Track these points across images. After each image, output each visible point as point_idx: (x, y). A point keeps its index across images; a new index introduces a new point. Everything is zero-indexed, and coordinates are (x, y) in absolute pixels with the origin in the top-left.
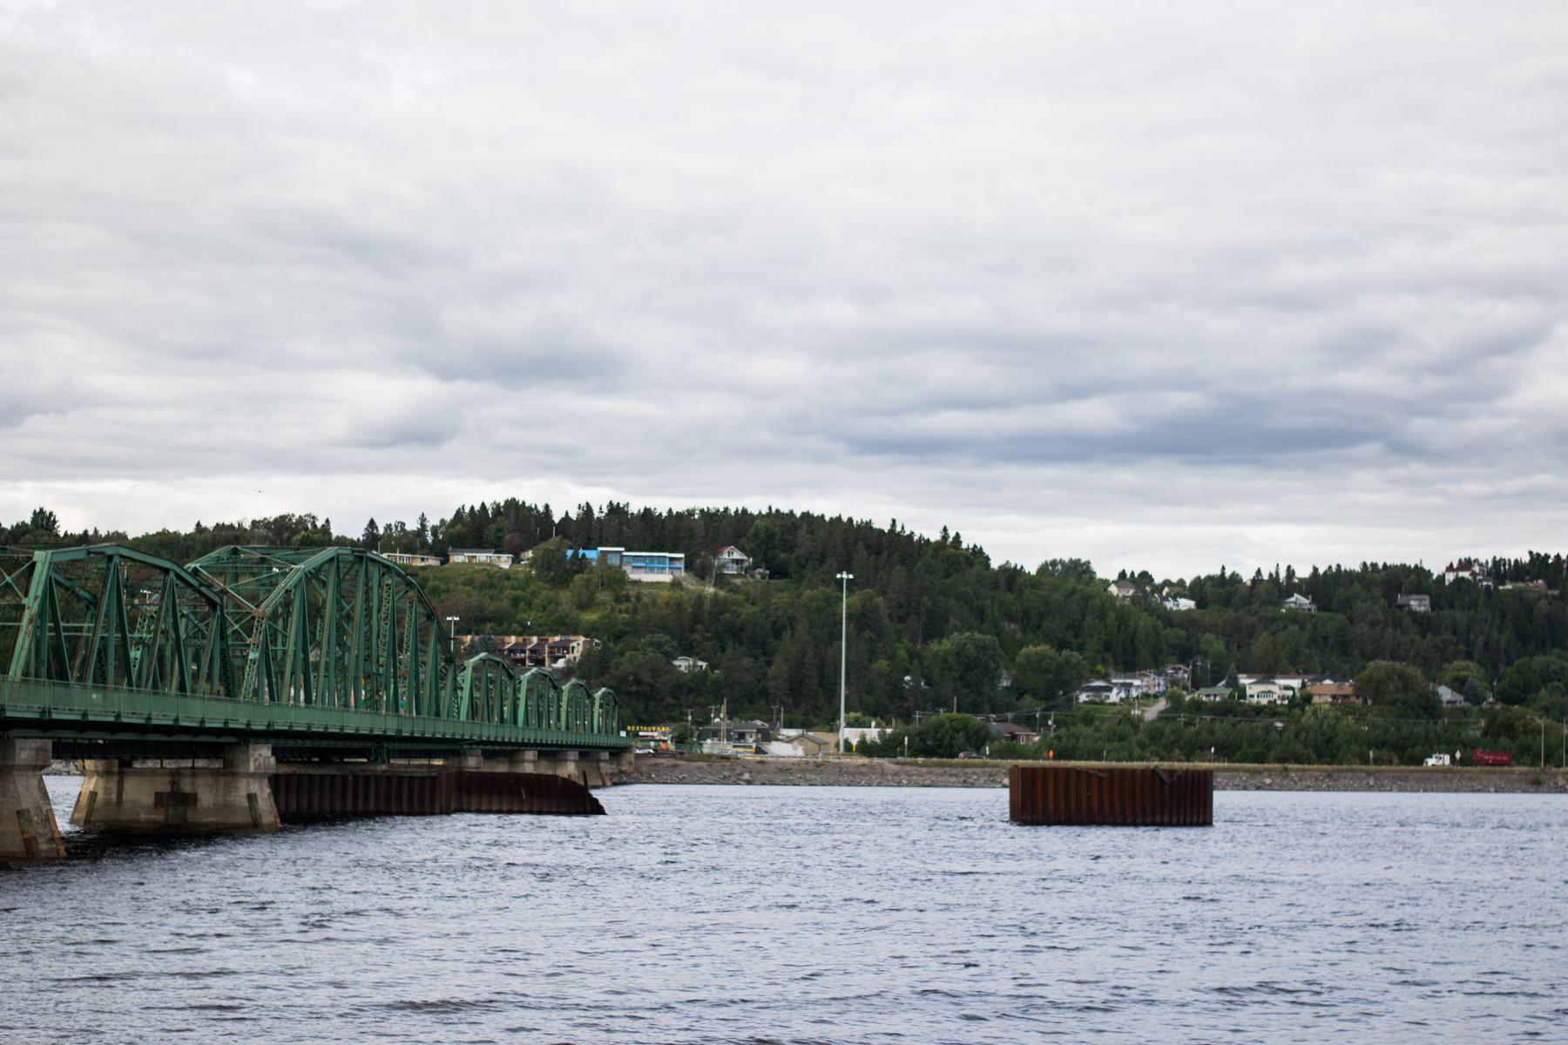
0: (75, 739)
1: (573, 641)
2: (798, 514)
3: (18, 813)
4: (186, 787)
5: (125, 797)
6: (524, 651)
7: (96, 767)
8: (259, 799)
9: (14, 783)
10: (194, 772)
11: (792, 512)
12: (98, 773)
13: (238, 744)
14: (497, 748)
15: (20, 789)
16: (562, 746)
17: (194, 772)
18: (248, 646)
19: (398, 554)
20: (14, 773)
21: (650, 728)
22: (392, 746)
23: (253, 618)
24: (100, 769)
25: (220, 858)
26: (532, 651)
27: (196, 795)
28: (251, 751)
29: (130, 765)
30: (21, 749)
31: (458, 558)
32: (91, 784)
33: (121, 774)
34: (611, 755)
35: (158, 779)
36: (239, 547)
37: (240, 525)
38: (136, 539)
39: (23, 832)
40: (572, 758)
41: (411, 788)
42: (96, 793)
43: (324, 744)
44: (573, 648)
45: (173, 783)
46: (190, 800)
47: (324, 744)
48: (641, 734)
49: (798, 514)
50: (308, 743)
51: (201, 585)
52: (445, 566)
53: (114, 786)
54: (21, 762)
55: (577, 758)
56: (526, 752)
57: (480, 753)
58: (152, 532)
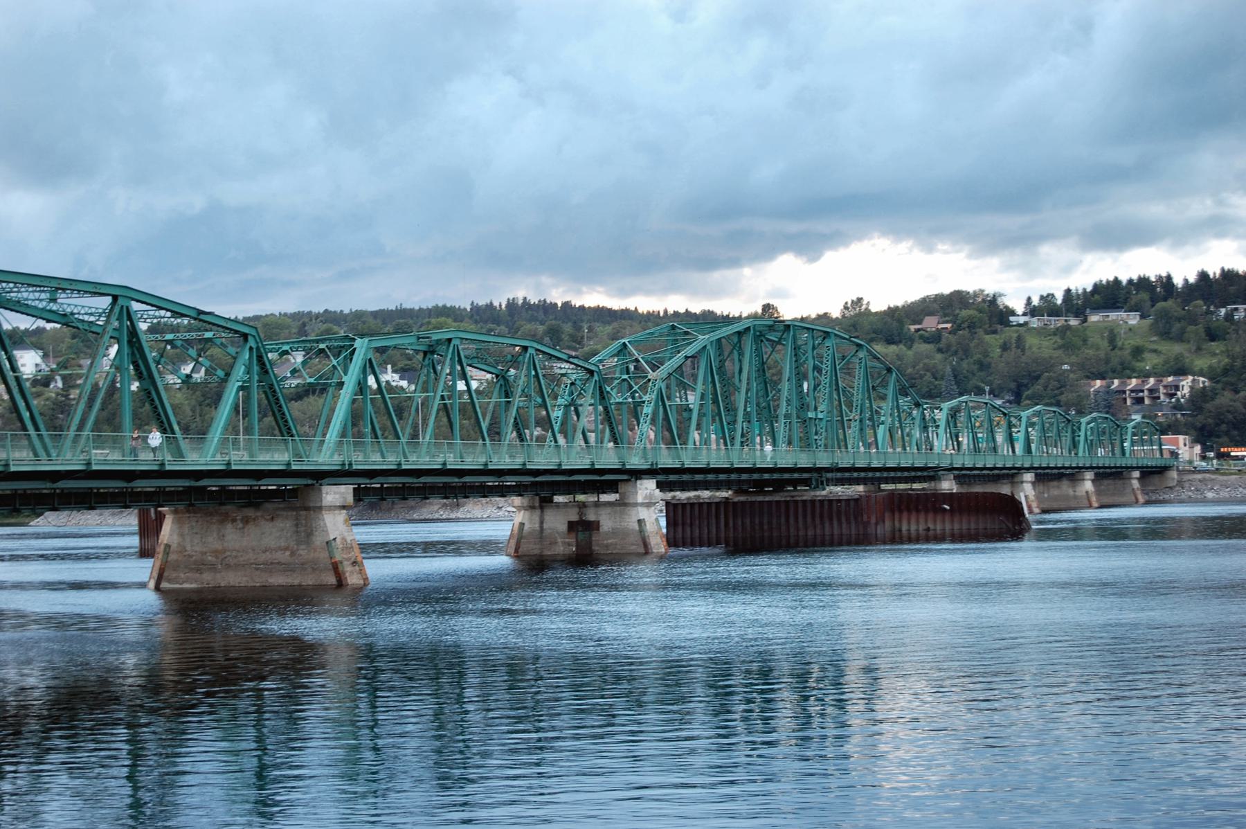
0: (251, 486)
1: (1182, 380)
2: (1124, 282)
3: (327, 543)
4: (591, 516)
5: (545, 526)
6: (1142, 391)
7: (522, 503)
8: (647, 524)
9: (324, 520)
10: (597, 504)
11: (1116, 279)
12: (525, 508)
13: (629, 480)
14: (1108, 470)
15: (328, 525)
16: (1127, 468)
17: (597, 504)
18: (644, 402)
19: (1046, 318)
20: (324, 512)
21: (1239, 449)
22: (829, 475)
23: (649, 380)
24: (525, 505)
25: (925, 559)
26: (1150, 390)
27: (599, 522)
28: (638, 486)
29: (551, 501)
30: (327, 493)
31: (1094, 318)
32: (520, 517)
33: (542, 508)
34: (359, 494)
35: (569, 510)
36: (675, 324)
37: (341, 311)
38: (876, 312)
39: (331, 558)
40: (1088, 477)
41: (805, 511)
42: (524, 524)
43: (776, 476)
44: (1183, 386)
45: (581, 514)
46: (592, 527)
47: (776, 476)
48: (1232, 454)
49: (1124, 282)
50: (913, 474)
51: (569, 358)
52: (1085, 324)
53: (536, 518)
54: (328, 504)
55: (350, 499)
56: (1025, 475)
57: (952, 476)
58: (900, 303)
